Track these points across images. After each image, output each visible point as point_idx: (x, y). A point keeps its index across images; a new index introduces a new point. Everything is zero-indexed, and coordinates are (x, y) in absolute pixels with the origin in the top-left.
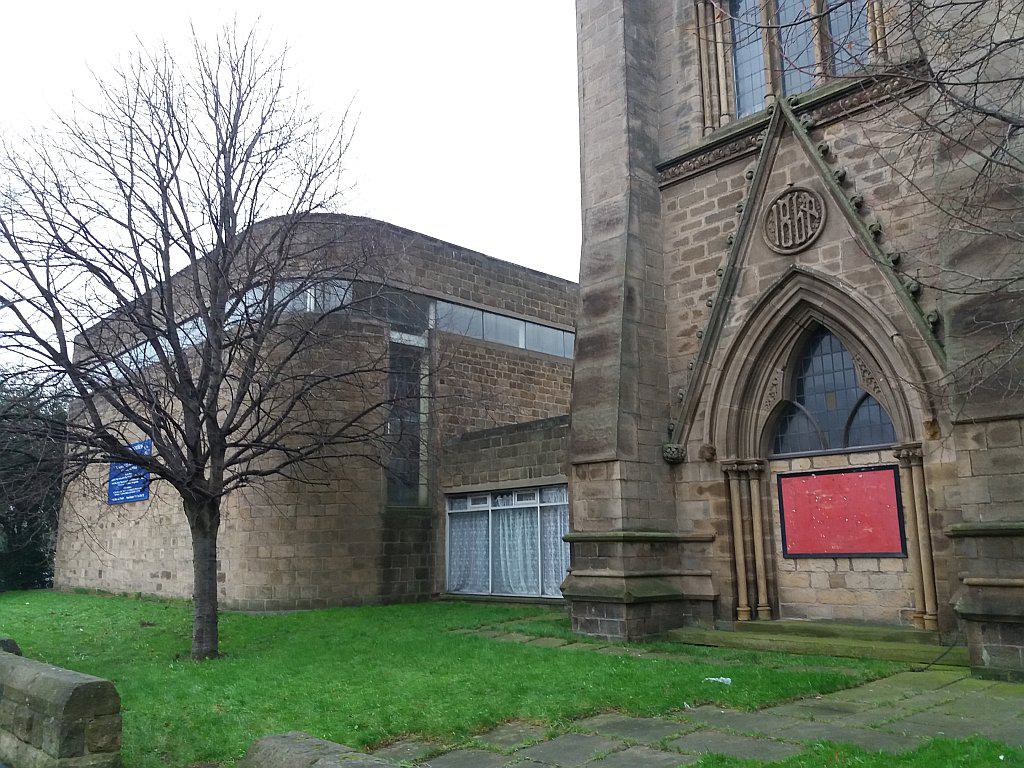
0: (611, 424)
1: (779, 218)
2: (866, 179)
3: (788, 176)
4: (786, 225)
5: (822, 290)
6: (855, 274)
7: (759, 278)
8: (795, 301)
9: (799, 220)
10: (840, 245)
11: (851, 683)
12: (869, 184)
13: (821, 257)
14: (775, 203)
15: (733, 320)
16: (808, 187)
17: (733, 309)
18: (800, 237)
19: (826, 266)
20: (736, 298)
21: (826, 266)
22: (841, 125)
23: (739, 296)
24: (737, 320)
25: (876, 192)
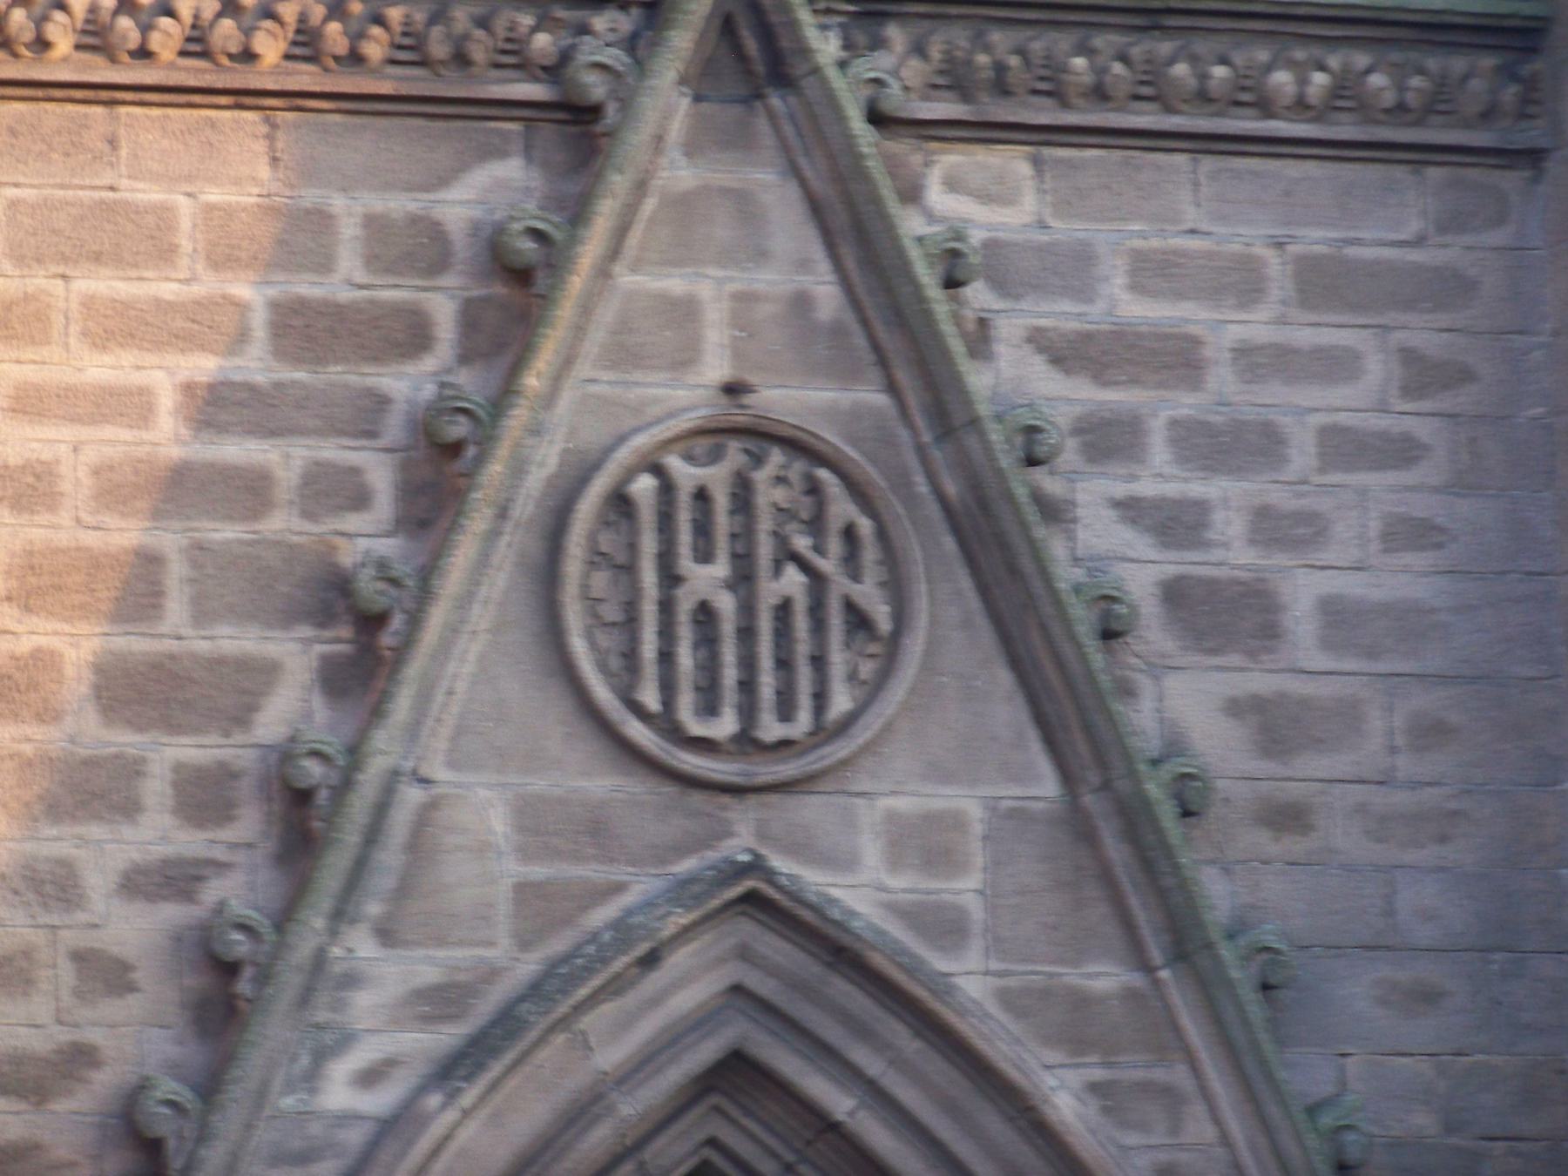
0: (170, 536)
1: (666, 560)
2: (1131, 509)
3: (715, 335)
4: (705, 614)
5: (863, 1032)
6: (1046, 994)
7: (513, 869)
8: (706, 1052)
9: (784, 609)
10: (974, 810)
11: (458, 429)
12: (1138, 543)
13: (871, 851)
14: (824, 733)
15: (342, 1069)
16: (831, 436)
17: (339, 1006)
18: (786, 711)
19: (895, 909)
20: (361, 945)
21: (895, 909)
22: (1013, 161)
23: (386, 935)
24: (369, 1078)
25: (1175, 594)
